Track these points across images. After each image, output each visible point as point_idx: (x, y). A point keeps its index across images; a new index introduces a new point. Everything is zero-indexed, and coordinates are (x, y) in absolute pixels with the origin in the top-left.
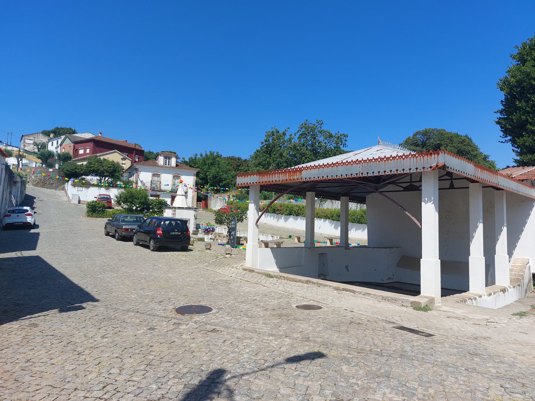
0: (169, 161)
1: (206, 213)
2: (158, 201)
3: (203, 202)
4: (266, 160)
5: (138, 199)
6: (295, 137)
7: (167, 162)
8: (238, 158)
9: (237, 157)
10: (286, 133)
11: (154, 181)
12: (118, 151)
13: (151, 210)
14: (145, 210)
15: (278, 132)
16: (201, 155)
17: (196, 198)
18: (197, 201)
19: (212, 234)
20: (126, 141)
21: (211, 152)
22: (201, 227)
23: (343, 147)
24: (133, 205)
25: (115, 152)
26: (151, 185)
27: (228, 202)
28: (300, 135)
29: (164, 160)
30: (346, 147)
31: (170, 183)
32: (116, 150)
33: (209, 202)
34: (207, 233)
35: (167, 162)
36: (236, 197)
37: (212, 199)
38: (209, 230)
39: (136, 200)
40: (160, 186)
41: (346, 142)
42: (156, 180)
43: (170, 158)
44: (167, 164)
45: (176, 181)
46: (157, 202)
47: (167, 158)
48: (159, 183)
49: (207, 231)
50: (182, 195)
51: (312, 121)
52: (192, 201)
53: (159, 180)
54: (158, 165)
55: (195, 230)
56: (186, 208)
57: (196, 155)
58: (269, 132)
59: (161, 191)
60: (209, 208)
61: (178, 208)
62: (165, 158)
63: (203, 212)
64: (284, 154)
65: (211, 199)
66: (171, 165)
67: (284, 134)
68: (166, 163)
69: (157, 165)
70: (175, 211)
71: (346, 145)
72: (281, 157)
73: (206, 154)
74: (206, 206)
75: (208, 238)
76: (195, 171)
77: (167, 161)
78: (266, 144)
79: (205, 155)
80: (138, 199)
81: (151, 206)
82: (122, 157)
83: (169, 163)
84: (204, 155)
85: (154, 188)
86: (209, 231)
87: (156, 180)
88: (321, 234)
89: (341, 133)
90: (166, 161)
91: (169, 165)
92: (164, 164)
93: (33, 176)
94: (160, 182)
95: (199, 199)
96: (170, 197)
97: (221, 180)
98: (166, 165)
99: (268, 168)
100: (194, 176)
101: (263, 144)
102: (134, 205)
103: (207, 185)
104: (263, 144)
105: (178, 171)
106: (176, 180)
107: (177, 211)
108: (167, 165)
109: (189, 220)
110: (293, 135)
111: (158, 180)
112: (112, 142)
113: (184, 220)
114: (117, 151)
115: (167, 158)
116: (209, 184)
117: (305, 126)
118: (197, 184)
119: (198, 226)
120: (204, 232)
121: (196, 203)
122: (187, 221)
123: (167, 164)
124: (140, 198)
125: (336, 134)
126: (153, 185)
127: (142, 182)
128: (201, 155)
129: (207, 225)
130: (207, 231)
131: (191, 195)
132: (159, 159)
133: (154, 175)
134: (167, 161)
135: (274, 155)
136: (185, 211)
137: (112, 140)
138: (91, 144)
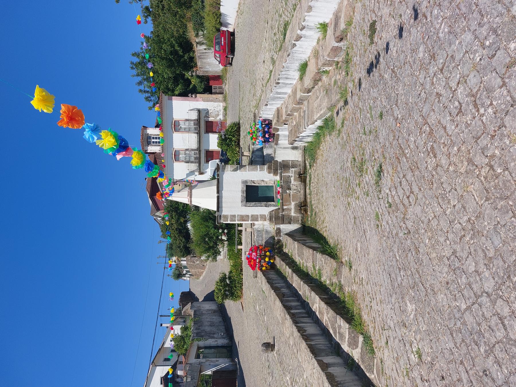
0: (153, 138)
3: (211, 83)
11: (185, 159)
17: (206, 96)
18: (211, 93)
26: (192, 162)
27: (207, 46)
29: (152, 146)
31: (186, 135)
33: (210, 74)
36: (197, 30)
37: (206, 70)
40: (192, 150)
42: (184, 156)
44: (158, 140)
45: (182, 126)
48: (187, 152)
50: (191, 197)
52: (212, 101)
53: (183, 152)
55: (266, 167)
56: (218, 192)
57: (141, 91)
59: (199, 149)
60: (221, 74)
62: (149, 143)
65: (207, 72)
68: (156, 142)
73: (138, 75)
74: (218, 78)
76: (165, 98)
77: (153, 140)
79: (139, 77)
83: (156, 138)
84: (140, 78)
85: (195, 158)
90: (153, 142)
92: (159, 146)
93: (197, 263)
94: (187, 150)
95: (208, 90)
96: (207, 135)
97: (174, 53)
98: (159, 142)
100: (171, 99)
105: (167, 125)
106: (181, 127)
113: (245, 195)
118: (184, 94)
122: (247, 187)
123: (158, 140)
127: (188, 175)
128: (140, 83)
131: (202, 103)
134: (153, 140)
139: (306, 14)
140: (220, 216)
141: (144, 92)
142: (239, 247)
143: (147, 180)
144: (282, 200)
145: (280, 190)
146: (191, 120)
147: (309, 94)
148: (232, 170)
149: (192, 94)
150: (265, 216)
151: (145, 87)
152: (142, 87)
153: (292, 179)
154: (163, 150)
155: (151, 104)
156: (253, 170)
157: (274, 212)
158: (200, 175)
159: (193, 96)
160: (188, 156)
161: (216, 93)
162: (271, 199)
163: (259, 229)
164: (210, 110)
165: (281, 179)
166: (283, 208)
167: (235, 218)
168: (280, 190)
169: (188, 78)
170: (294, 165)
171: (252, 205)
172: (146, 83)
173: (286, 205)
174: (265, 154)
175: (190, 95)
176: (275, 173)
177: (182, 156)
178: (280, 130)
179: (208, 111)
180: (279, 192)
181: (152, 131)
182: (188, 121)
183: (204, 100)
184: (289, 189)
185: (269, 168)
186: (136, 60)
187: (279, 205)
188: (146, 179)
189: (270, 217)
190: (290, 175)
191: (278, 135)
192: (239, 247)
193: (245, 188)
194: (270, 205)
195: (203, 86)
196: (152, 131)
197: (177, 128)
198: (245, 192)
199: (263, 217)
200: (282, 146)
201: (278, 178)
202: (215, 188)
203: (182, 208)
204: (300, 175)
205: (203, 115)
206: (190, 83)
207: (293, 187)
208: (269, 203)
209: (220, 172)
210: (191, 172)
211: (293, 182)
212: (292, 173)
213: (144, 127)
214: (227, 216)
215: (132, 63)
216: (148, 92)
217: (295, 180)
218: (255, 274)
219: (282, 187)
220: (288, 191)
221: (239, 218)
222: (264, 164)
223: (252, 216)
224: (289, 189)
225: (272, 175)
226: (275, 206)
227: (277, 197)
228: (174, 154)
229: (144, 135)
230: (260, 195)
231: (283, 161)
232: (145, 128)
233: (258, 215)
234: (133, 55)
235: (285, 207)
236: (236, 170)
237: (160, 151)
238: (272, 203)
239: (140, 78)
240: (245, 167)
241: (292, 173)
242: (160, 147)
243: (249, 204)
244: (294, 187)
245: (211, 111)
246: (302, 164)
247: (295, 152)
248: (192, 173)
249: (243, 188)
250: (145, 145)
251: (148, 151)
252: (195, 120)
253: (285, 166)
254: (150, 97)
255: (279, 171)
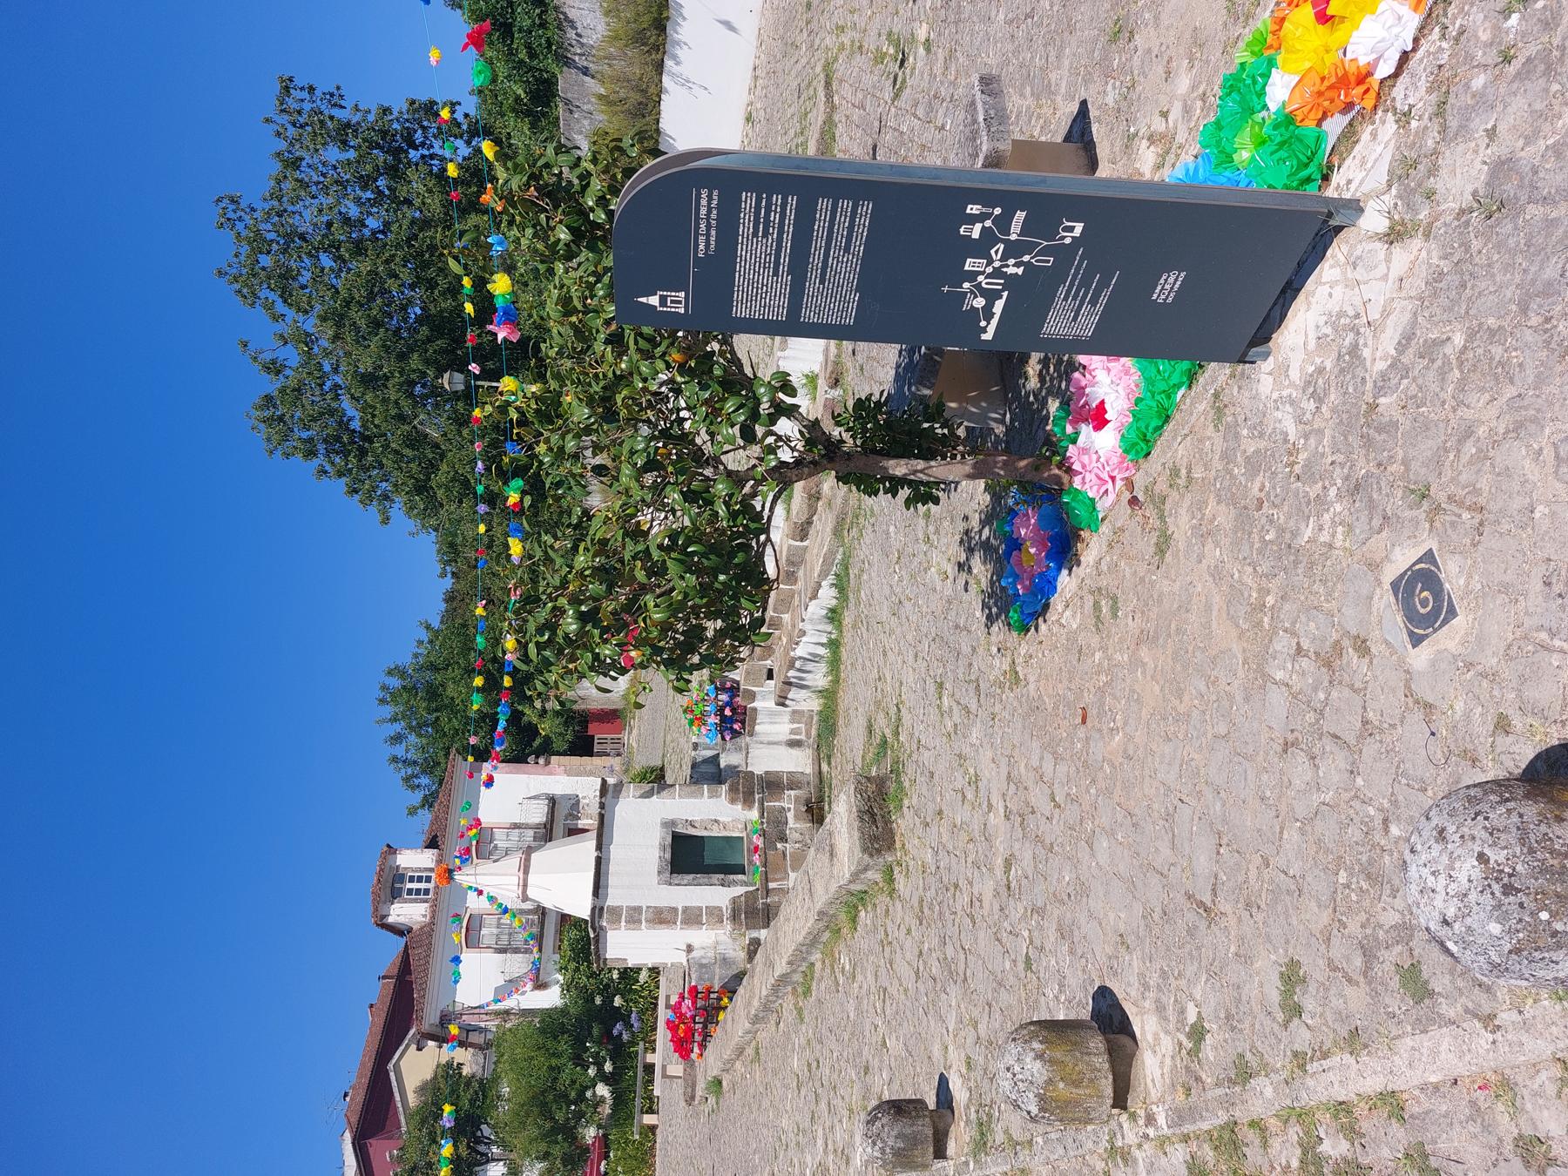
0: (412, 879)
1: (640, 718)
2: (573, 965)
3: (593, 728)
4: (396, 452)
5: (558, 1069)
6: (289, 319)
7: (415, 886)
8: (446, 601)
9: (443, 606)
10: (267, 356)
12: (391, 1058)
13: (618, 1001)
14: (615, 1032)
15: (269, 399)
16: (397, 739)
17: (576, 760)
18: (590, 753)
19: (752, 696)
20: (371, 1006)
21: (382, 701)
22: (709, 753)
23: (342, 107)
24: (589, 1094)
25: (397, 1067)
26: (516, 951)
28: (285, 301)
30: (341, 96)
32: (390, 1066)
34: (743, 722)
35: (415, 886)
38: (728, 712)
39: (565, 1077)
41: (318, 93)
42: (495, 931)
43: (399, 877)
44: (423, 886)
45: (500, 844)
46: (577, 970)
47: (393, 885)
49: (731, 720)
50: (526, 872)
51: (226, 248)
54: (430, 924)
55: (724, 788)
56: (599, 847)
57: (395, 759)
58: (269, 440)
61: (597, 891)
62: (395, 895)
63: (635, 732)
64: (366, 365)
66: (431, 870)
67: (275, 368)
68: (418, 891)
69: (429, 929)
70: (616, 912)
71: (332, 95)
72: (377, 378)
73: (394, 719)
75: (772, 714)
77: (409, 886)
78: (327, 454)
80: (558, 1069)
81: (598, 1001)
82: (414, 1047)
83: (420, 879)
86: (733, 710)
87: (495, 931)
88: (749, 119)
89: (271, 108)
90: (410, 892)
91: (428, 880)
92: (425, 901)
95: (582, 746)
98: (427, 892)
99: (437, 446)
101: (328, 467)
102: (587, 1088)
103: (523, 714)
104: (328, 467)
106: (496, 847)
107: (614, 899)
108: (431, 886)
109: (669, 824)
110: (280, 327)
111: (494, 922)
112: (370, 1065)
113: (668, 856)
114: (394, 1061)
115: (393, 885)
116: (520, 708)
117: (248, 283)
118: (518, 757)
119: (703, 769)
120: (736, 734)
121: (596, 761)
123: (423, 886)
124: (554, 1062)
125: (278, 134)
126: (515, 944)
128: (397, 739)
129: (700, 720)
130: (731, 720)
131: (564, 779)
132: (401, 920)
133: (472, 940)
134: (409, 886)
135: (374, 416)
136: (616, 852)
137: (363, 1064)
138: (375, 1146)
139: (780, 354)
140: (602, 909)
141: (404, 762)
142: (649, 1119)
143: (348, 1099)
144: (765, 865)
145: (760, 843)
146: (527, 827)
147: (805, 544)
148: (638, 794)
149: (537, 757)
150: (720, 909)
151: (407, 751)
152: (399, 750)
153: (790, 815)
154: (433, 917)
155: (418, 797)
156: (691, 795)
157: (743, 899)
158: (537, 992)
159: (541, 761)
160: (507, 931)
161: (600, 754)
162: (740, 870)
163: (704, 961)
164: (584, 798)
165: (762, 816)
166: (767, 886)
167: (640, 914)
168: (760, 843)
169: (530, 723)
170: (794, 783)
171: (685, 882)
172: (413, 738)
173: (776, 880)
174: (722, 765)
175: (531, 759)
176: (748, 802)
177: (488, 932)
178: (758, 697)
179: (578, 802)
180: (756, 849)
181: (414, 859)
182: (519, 828)
183: (569, 773)
184: (784, 839)
185: (733, 790)
186: (395, 683)
187: (757, 877)
188: (346, 1095)
189: (734, 910)
190: (786, 806)
191: (755, 710)
192: (649, 1119)
193: (669, 839)
194: (735, 883)
195: (569, 737)
196: (414, 859)
197: (485, 849)
198: (669, 850)
199: (715, 914)
200: (766, 739)
201: (754, 814)
202: (594, 843)
203: (467, 1106)
204: (808, 803)
205: (561, 812)
206: (537, 733)
207: (792, 835)
208: (731, 877)
209: (608, 799)
210: (510, 981)
211: (791, 823)
212: (789, 802)
213: (388, 846)
214: (620, 908)
215: (384, 688)
216: (415, 763)
217: (796, 817)
218: (689, 1090)
219: (764, 834)
220: (779, 846)
221: (651, 916)
222: (721, 783)
223: (686, 909)
224: (784, 839)
225: (739, 807)
226: (746, 884)
227: (751, 862)
228: (464, 924)
229: (387, 871)
230: (707, 862)
231: (766, 773)
232: (392, 850)
233: (700, 909)
234: (390, 673)
235: (772, 885)
236: (648, 795)
237: (425, 916)
238: (740, 877)
239: (398, 727)
240: (672, 789)
241: (789, 802)
242: (426, 905)
243: (677, 878)
244: (796, 836)
245: (587, 801)
246: (813, 780)
247: (795, 752)
248: (512, 986)
249: (664, 839)
250: (383, 899)
251: (391, 920)
252: (537, 827)
253: (772, 784)
254: (417, 776)
255: (757, 796)
